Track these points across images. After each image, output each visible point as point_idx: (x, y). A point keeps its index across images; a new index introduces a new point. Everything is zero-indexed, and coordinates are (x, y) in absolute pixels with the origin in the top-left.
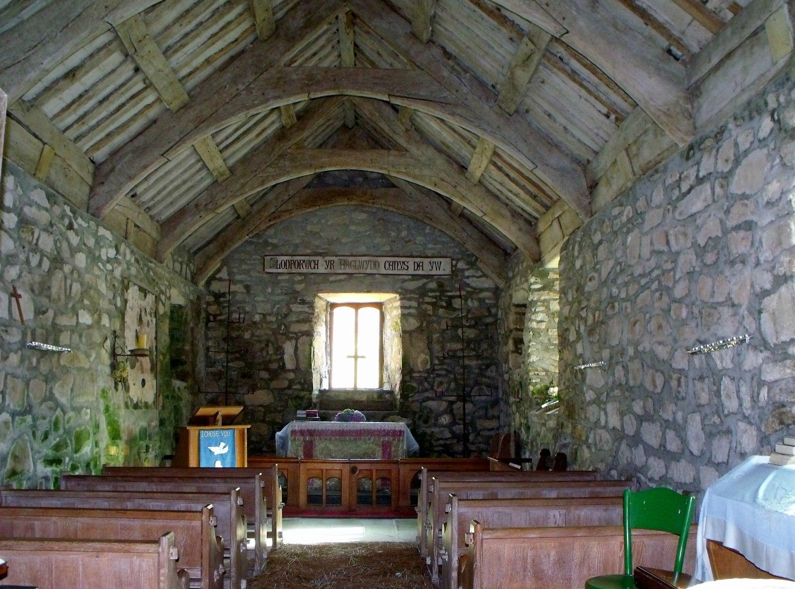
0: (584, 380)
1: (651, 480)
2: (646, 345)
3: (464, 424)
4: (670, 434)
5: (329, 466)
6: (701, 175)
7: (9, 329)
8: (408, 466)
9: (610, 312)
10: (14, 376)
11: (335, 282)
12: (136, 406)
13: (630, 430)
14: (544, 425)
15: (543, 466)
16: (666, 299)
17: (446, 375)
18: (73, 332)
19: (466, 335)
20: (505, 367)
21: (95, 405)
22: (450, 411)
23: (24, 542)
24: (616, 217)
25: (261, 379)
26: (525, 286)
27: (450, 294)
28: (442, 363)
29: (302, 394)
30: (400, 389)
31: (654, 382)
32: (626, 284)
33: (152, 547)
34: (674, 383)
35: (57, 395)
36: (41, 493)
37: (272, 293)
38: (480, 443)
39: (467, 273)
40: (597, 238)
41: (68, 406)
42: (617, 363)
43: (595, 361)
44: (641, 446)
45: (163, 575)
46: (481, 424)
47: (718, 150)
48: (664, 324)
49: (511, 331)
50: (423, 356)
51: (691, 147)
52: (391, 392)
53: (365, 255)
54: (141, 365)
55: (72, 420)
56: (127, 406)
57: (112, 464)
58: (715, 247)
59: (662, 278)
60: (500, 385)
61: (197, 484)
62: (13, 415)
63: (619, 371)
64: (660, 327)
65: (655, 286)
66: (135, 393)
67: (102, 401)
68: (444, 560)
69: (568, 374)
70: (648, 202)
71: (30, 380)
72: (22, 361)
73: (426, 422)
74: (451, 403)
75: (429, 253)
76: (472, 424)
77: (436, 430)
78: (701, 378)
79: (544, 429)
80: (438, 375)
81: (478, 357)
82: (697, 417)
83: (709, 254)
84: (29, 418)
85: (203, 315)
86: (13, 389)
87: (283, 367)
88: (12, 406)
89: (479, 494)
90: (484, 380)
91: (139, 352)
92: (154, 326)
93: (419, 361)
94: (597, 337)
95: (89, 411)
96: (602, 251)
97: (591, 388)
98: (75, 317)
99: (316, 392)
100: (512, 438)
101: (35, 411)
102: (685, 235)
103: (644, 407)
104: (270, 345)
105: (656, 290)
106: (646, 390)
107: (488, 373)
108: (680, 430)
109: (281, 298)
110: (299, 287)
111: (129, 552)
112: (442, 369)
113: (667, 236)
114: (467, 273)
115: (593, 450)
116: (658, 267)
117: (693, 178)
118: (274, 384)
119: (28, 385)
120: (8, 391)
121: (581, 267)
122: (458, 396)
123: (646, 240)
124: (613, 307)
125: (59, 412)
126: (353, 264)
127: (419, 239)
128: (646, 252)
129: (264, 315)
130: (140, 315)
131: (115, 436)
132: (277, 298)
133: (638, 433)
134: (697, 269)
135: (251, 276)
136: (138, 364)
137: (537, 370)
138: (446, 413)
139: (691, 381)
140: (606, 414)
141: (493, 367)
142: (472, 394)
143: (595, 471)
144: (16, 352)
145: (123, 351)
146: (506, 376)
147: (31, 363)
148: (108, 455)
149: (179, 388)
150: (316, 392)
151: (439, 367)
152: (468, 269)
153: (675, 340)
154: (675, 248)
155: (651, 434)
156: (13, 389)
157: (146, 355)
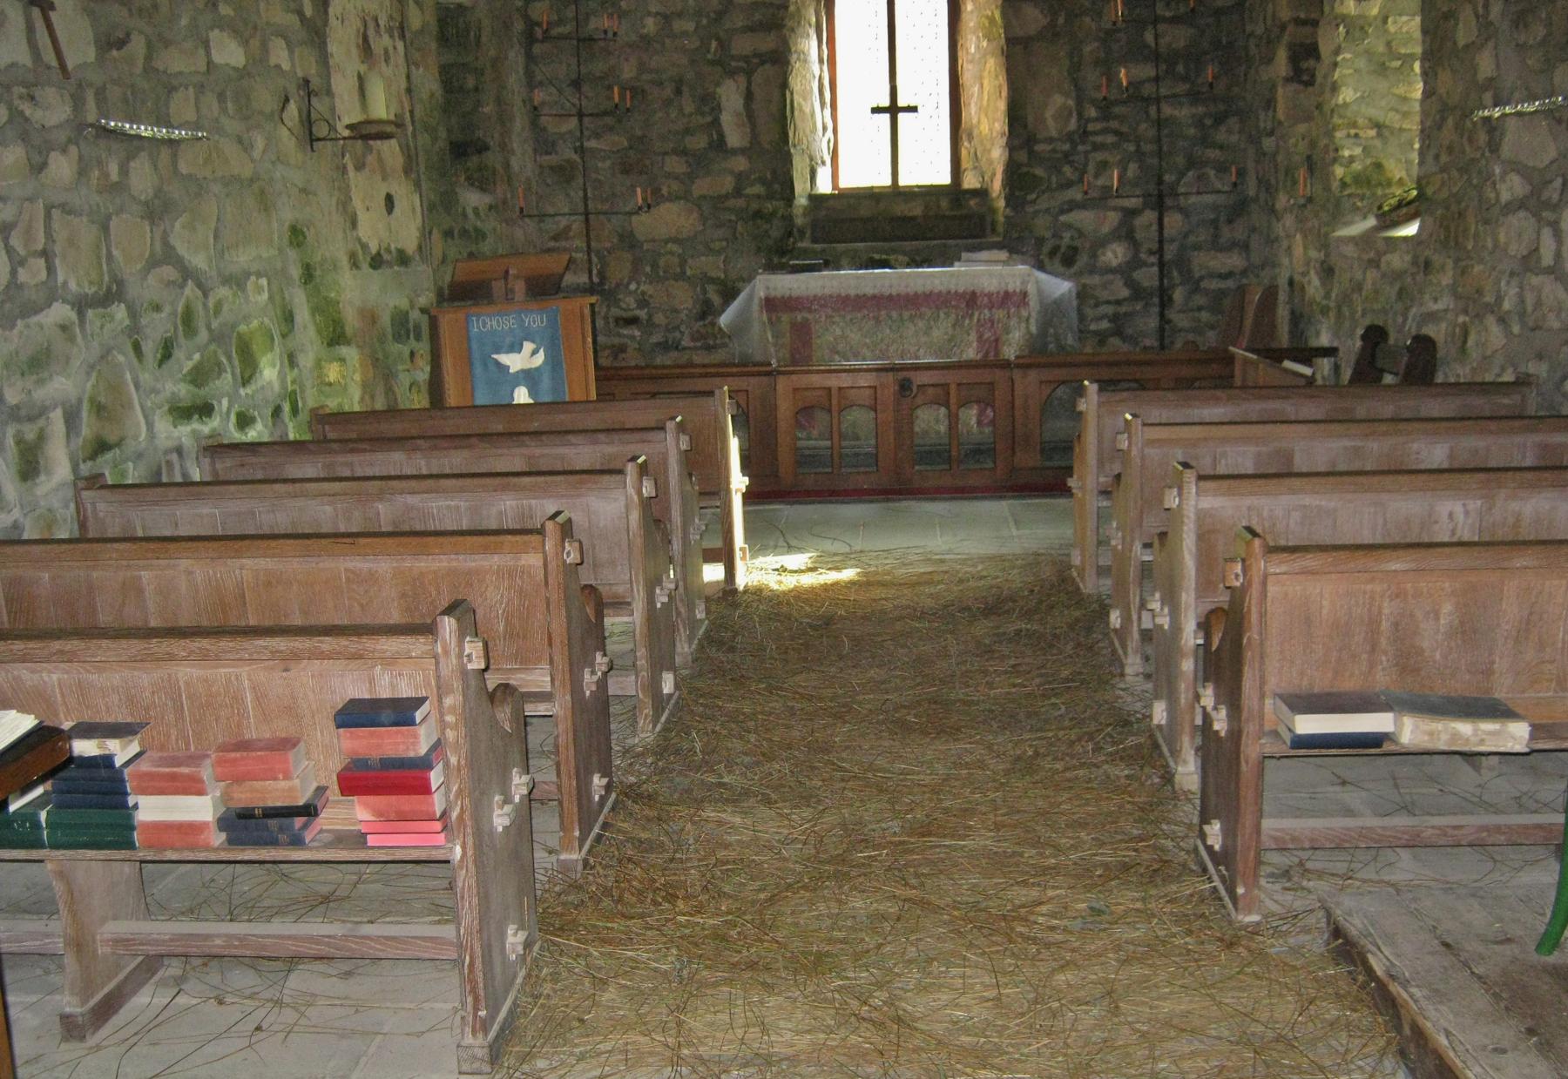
0: (1494, 147)
5: (845, 381)
7: (38, 93)
8: (1033, 375)
10: (66, 209)
12: (377, 262)
14: (1374, 263)
15: (1367, 372)
17: (1116, 146)
18: (200, 89)
20: (1264, 121)
21: (279, 265)
22: (1125, 232)
23: (105, 643)
25: (669, 175)
28: (1106, 114)
29: (769, 206)
30: (1004, 186)
33: (417, 645)
35: (182, 249)
36: (172, 492)
38: (1200, 309)
41: (214, 273)
43: (1532, 98)
45: (452, 710)
46: (1207, 262)
49: (1283, 28)
50: (1058, 100)
52: (982, 193)
54: (380, 160)
55: (225, 308)
56: (355, 265)
57: (332, 404)
60: (1251, 165)
61: (524, 451)
62: (81, 305)
66: (373, 230)
67: (292, 254)
69: (1448, 134)
71: (109, 218)
72: (82, 172)
74: (1131, 213)
76: (1182, 262)
79: (1372, 275)
80: (1097, 147)
81: (1195, 97)
84: (120, 312)
85: (519, 26)
86: (71, 242)
88: (73, 286)
89: (1242, 458)
90: (1213, 154)
91: (373, 129)
92: (401, 60)
93: (1049, 114)
94: (1541, 31)
95: (264, 281)
97: (1515, 166)
98: (202, 52)
99: (801, 201)
100: (1282, 296)
101: (133, 291)
104: (685, 89)
107: (1221, 136)
111: (361, 657)
112: (1105, 131)
115: (1516, 329)
118: (701, 187)
119: (105, 228)
120: (58, 249)
122: (1147, 196)
125: (190, 289)
130: (365, 39)
131: (336, 337)
136: (370, 159)
137: (1354, 125)
138: (1119, 238)
140: (1558, 234)
141: (1233, 122)
142: (1182, 190)
143: (1522, 382)
144: (64, 151)
145: (332, 128)
146: (1268, 143)
147: (107, 175)
148: (324, 385)
149: (476, 210)
150: (801, 201)
156: (71, 242)
157: (388, 136)
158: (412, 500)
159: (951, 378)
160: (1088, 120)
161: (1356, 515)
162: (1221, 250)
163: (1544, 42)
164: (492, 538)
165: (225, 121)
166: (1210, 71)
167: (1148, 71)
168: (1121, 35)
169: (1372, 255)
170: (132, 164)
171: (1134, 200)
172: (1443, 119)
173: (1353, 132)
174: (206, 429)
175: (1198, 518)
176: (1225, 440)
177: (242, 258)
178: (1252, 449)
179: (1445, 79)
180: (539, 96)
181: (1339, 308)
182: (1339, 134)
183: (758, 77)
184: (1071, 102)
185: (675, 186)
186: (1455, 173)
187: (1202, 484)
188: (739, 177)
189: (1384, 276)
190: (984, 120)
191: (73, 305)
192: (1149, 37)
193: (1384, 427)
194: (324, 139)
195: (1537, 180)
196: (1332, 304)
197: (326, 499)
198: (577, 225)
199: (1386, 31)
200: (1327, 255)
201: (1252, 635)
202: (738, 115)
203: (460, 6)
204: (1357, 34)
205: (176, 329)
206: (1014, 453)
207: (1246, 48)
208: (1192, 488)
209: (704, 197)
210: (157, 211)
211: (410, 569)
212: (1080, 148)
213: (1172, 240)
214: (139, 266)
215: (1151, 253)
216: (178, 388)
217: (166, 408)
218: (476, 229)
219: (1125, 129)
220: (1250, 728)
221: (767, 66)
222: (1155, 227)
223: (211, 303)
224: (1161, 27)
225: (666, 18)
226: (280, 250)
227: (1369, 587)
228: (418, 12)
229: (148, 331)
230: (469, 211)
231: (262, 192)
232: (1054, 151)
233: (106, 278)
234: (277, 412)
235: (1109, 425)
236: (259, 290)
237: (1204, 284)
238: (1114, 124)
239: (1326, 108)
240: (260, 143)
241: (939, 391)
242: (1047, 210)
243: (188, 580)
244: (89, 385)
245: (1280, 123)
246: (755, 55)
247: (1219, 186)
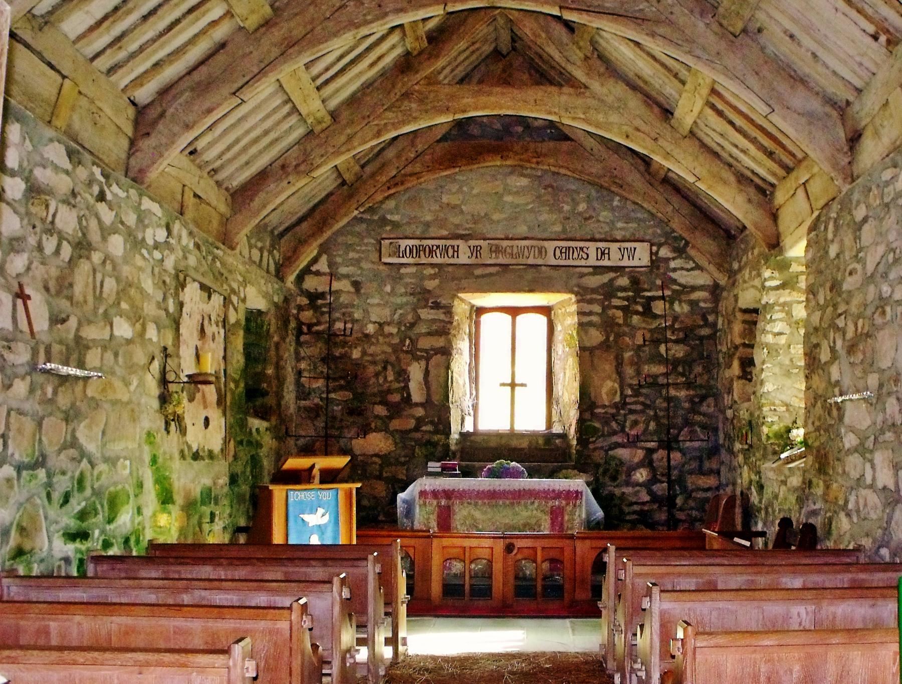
0: (841, 418)
3: (670, 482)
7: (13, 345)
10: (20, 412)
11: (483, 276)
12: (196, 456)
14: (784, 483)
20: (727, 400)
22: (647, 462)
23: (35, 652)
24: (887, 183)
26: (757, 282)
28: (636, 394)
29: (436, 438)
30: (576, 432)
33: (219, 659)
35: (82, 440)
36: (60, 582)
38: (692, 509)
39: (673, 264)
40: (860, 213)
41: (99, 455)
50: (609, 384)
52: (564, 436)
53: (525, 238)
54: (204, 396)
56: (183, 456)
57: (161, 540)
60: (721, 425)
62: (19, 469)
67: (146, 448)
71: (42, 418)
72: (32, 391)
74: (650, 451)
75: (618, 235)
76: (681, 481)
77: (628, 490)
79: (783, 488)
80: (632, 412)
81: (689, 385)
84: (42, 473)
85: (293, 324)
86: (19, 431)
87: (407, 400)
88: (17, 456)
89: (690, 583)
90: (698, 418)
91: (201, 378)
93: (604, 391)
95: (128, 462)
96: (867, 232)
98: (108, 328)
99: (455, 436)
101: (52, 462)
109: (404, 299)
110: (431, 285)
112: (636, 403)
114: (673, 264)
115: (855, 520)
118: (395, 424)
119: (40, 425)
120: (11, 434)
121: (838, 256)
122: (660, 441)
124: (884, 313)
126: (509, 250)
127: (605, 215)
130: (202, 325)
131: (166, 499)
132: (399, 300)
136: (198, 396)
137: (774, 404)
140: (873, 467)
141: (711, 400)
142: (681, 438)
144: (23, 378)
145: (177, 376)
146: (729, 413)
147: (45, 394)
148: (157, 527)
149: (257, 430)
150: (455, 436)
151: (633, 400)
152: (674, 259)
156: (19, 431)
157: (210, 383)
159: (539, 544)
160: (626, 396)
161: (747, 613)
162: (704, 475)
163: (862, 362)
164: (261, 611)
165: (117, 368)
166: (698, 369)
167: (662, 369)
168: (647, 349)
169: (783, 478)
170: (60, 389)
171: (653, 444)
172: (816, 402)
173: (773, 408)
174: (83, 548)
175: (661, 612)
177: (116, 448)
179: (816, 380)
180: (303, 365)
181: (766, 508)
182: (765, 409)
183: (432, 362)
184: (616, 385)
185: (379, 423)
186: (822, 432)
187: (663, 595)
189: (789, 490)
190: (566, 394)
191: (15, 467)
192: (662, 349)
194: (172, 382)
196: (763, 506)
197: (152, 590)
199: (790, 353)
200: (760, 478)
202: (420, 383)
203: (259, 311)
204: (774, 354)
205: (73, 486)
206: (575, 591)
207: (718, 359)
209: (397, 431)
210: (70, 416)
211: (212, 627)
212: (622, 412)
213: (675, 468)
214: (56, 448)
215: (663, 475)
216: (69, 521)
217: (61, 533)
218: (257, 441)
219: (648, 402)
221: (439, 356)
222: (665, 460)
223: (96, 473)
224: (669, 345)
225: (381, 325)
226: (140, 446)
227: (753, 656)
228: (235, 313)
229: (56, 486)
230: (254, 430)
231: (133, 411)
232: (606, 413)
233: (37, 453)
234: (127, 541)
235: (625, 570)
236: (125, 467)
237: (694, 494)
238: (641, 399)
239: (758, 394)
240: (135, 383)
241: (531, 551)
242: (602, 448)
243: (80, 625)
244: (18, 516)
245: (735, 402)
246: (432, 349)
247: (702, 437)
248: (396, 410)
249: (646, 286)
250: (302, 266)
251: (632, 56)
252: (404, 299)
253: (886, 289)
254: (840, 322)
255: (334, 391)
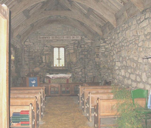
1: (133, 87)
2: (131, 57)
3: (85, 74)
4: (138, 77)
6: (146, 18)
9: (122, 49)
11: (54, 42)
13: (127, 76)
16: (136, 46)
19: (85, 53)
24: (123, 27)
26: (99, 42)
27: (81, 44)
28: (79, 60)
31: (134, 66)
32: (126, 43)
34: (139, 66)
37: (39, 45)
39: (85, 39)
40: (118, 32)
42: (124, 61)
44: (130, 80)
47: (150, 12)
48: (136, 52)
49: (96, 52)
51: (143, 11)
53: (61, 35)
58: (149, 35)
59: (136, 42)
63: (124, 62)
64: (135, 53)
65: (134, 43)
68: (87, 107)
70: (132, 23)
73: (76, 74)
74: (82, 69)
75: (76, 34)
77: (78, 76)
78: (146, 65)
80: (78, 63)
82: (145, 73)
83: (148, 36)
87: (42, 62)
89: (94, 92)
96: (120, 35)
102: (142, 32)
103: (131, 71)
105: (134, 44)
106: (132, 67)
107: (90, 62)
108: (140, 76)
109: (42, 46)
110: (46, 43)
113: (137, 32)
114: (85, 39)
116: (134, 39)
117: (144, 18)
118: (41, 66)
121: (114, 38)
123: (131, 32)
124: (123, 48)
126: (58, 37)
127: (74, 31)
128: (131, 35)
129: (38, 50)
132: (41, 46)
133: (129, 77)
134: (145, 40)
135: (34, 41)
139: (143, 65)
140: (121, 72)
151: (79, 61)
152: (85, 38)
153: (139, 56)
154: (139, 35)
155: (133, 77)
158: (18, 95)
169: (105, 74)
175: (91, 97)
176: (93, 90)
178: (95, 91)
188: (44, 65)
193: (106, 89)
195: (119, 67)
198: (28, 69)
201: (99, 107)
208: (90, 94)
220: (99, 115)
238: (80, 61)
242: (74, 69)
248: (40, 64)
249: (80, 43)
250: (25, 40)
251: (82, 8)
252: (42, 46)
253: (123, 44)
254: (115, 49)
255: (30, 61)
